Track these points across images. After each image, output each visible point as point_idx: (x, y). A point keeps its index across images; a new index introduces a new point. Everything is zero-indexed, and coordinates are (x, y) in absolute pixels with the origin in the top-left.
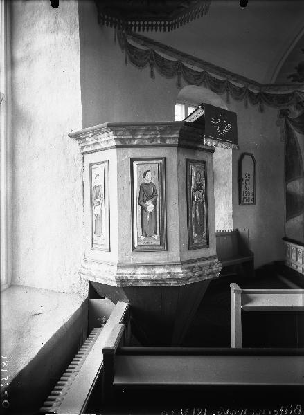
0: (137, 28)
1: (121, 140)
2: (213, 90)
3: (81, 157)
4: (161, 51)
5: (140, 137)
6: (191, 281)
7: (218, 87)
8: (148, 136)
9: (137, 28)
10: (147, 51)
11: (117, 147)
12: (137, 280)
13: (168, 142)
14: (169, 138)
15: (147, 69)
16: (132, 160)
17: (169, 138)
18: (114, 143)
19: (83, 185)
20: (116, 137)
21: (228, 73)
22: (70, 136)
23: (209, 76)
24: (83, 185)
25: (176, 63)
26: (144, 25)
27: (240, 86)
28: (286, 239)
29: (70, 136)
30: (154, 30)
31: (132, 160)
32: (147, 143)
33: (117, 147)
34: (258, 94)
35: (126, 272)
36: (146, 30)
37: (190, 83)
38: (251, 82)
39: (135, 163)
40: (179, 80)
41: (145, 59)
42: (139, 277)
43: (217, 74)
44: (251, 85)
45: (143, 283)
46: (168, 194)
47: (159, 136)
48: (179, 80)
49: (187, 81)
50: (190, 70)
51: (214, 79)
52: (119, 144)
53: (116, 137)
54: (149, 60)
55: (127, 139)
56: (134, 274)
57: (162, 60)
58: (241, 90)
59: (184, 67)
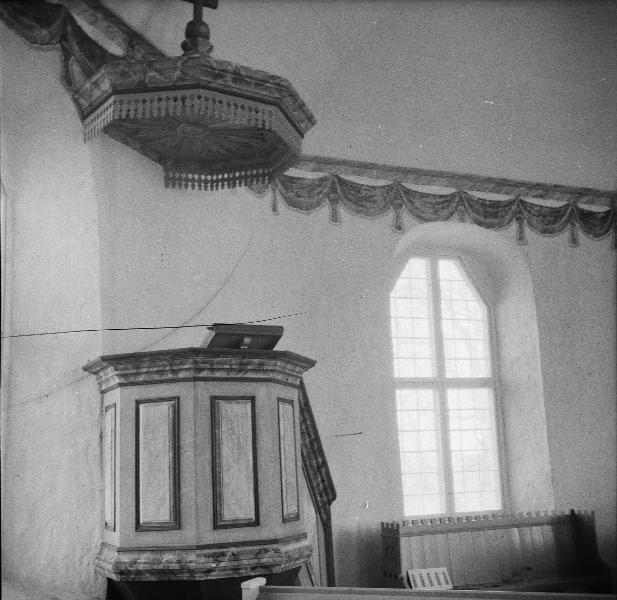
0: (190, 184)
1: (124, 376)
2: (480, 224)
3: (99, 396)
4: (354, 173)
5: (145, 370)
6: (213, 576)
7: (495, 215)
8: (155, 369)
9: (190, 184)
10: (322, 180)
11: (121, 385)
12: (139, 572)
13: (181, 375)
14: (182, 370)
15: (325, 210)
16: (138, 403)
17: (182, 370)
18: (117, 380)
19: (101, 437)
20: (117, 373)
21: (518, 184)
22: (86, 369)
23: (470, 199)
24: (101, 437)
25: (390, 188)
26: (187, 180)
27: (551, 203)
28: (283, 519)
29: (86, 369)
30: (197, 188)
31: (138, 403)
32: (156, 377)
33: (121, 385)
34: (607, 213)
35: (126, 558)
36: (209, 188)
37: (423, 219)
38: (583, 193)
39: (141, 407)
40: (398, 217)
41: (321, 192)
42: (141, 567)
43: (491, 191)
44: (585, 199)
45: (148, 575)
46: (116, 454)
47: (168, 368)
48: (398, 217)
49: (419, 217)
50: (423, 195)
51: (483, 203)
52: (123, 381)
53: (117, 373)
54: (327, 195)
55: (132, 375)
56: (135, 563)
57: (356, 187)
58: (556, 213)
59: (408, 192)
